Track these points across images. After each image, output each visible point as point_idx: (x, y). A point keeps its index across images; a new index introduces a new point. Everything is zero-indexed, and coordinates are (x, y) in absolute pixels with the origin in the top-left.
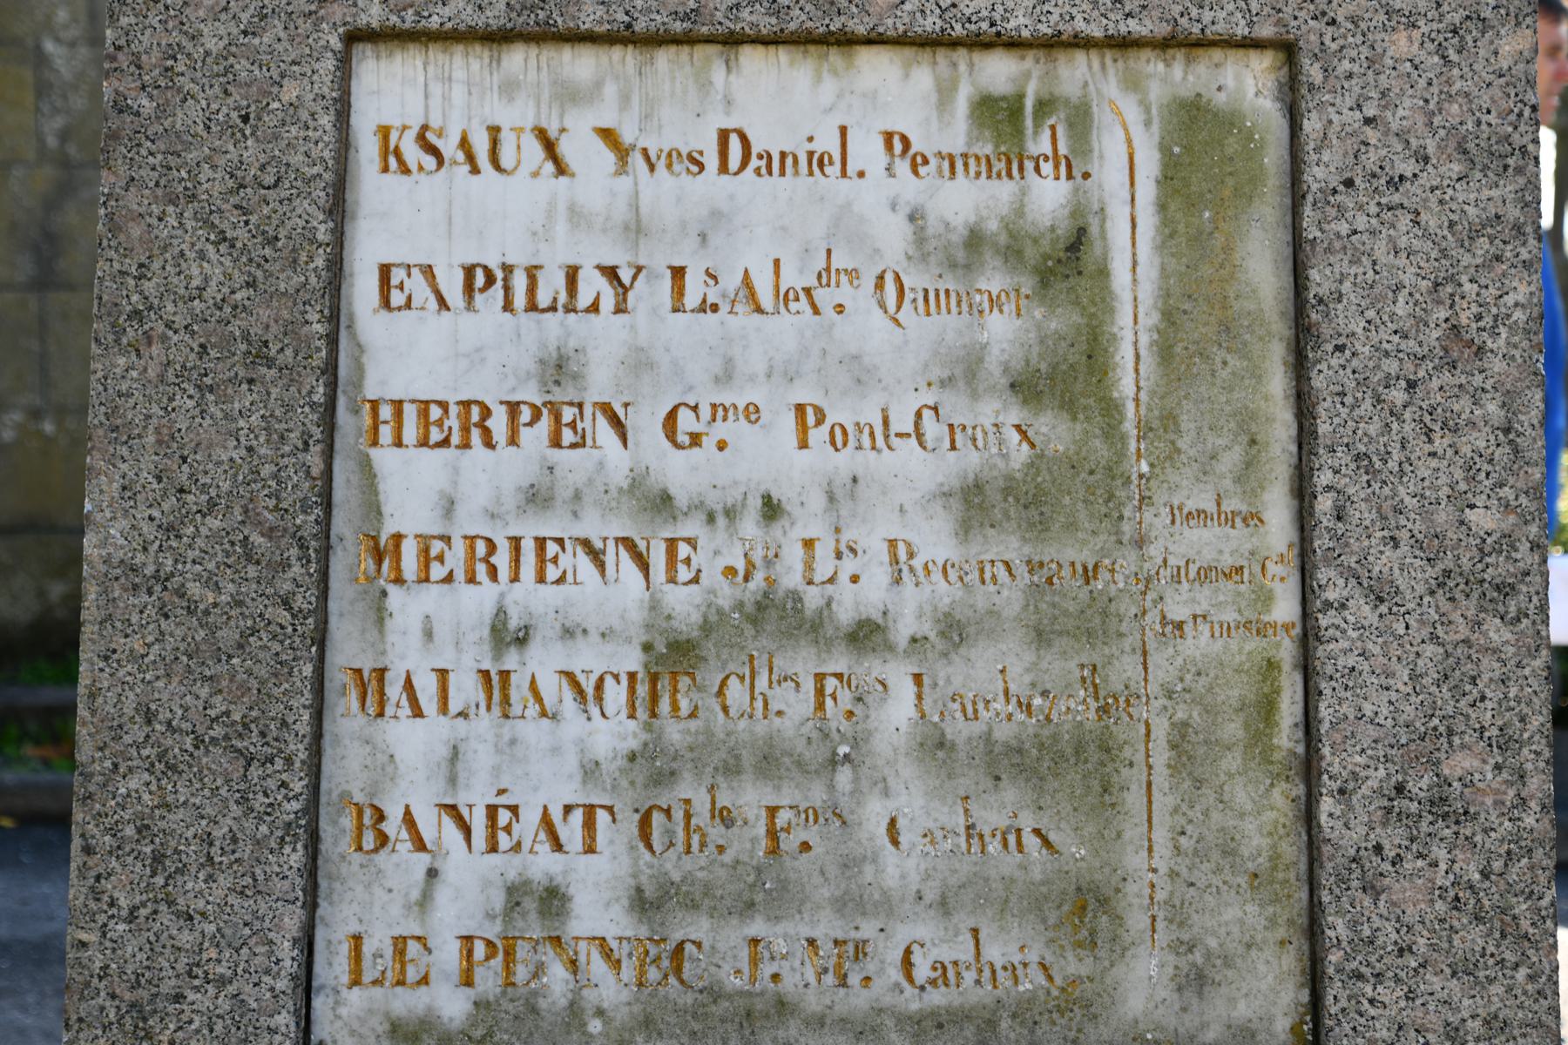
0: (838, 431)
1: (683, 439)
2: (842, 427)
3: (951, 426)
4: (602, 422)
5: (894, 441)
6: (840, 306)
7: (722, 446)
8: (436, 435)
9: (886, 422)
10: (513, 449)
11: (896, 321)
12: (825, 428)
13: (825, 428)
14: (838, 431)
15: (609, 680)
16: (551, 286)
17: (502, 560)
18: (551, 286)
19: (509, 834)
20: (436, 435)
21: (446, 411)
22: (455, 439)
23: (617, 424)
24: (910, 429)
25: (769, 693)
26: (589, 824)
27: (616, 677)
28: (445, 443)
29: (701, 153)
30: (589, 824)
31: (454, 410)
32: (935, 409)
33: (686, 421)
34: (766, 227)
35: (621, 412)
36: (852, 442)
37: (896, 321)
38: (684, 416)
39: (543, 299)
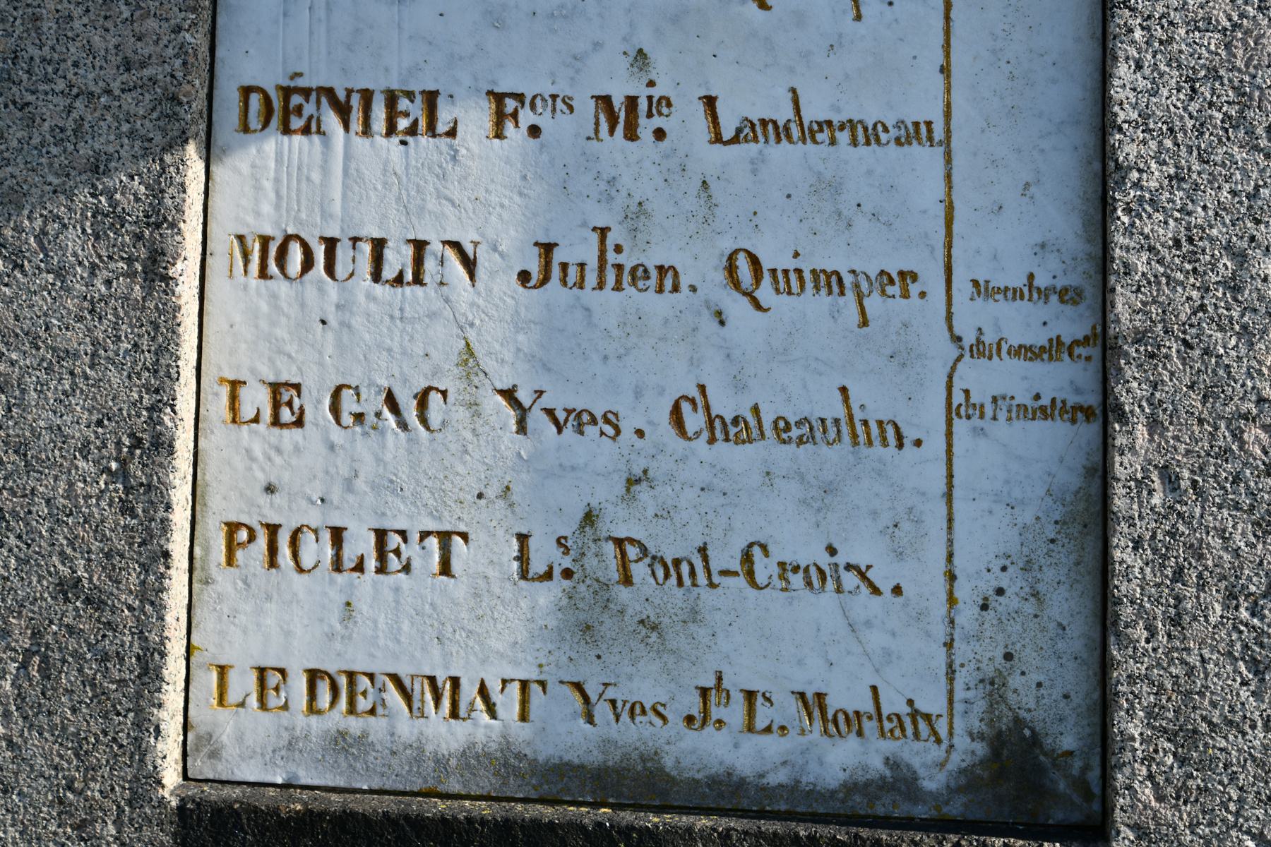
3: (782, 565)
24: (736, 565)
32: (764, 548)
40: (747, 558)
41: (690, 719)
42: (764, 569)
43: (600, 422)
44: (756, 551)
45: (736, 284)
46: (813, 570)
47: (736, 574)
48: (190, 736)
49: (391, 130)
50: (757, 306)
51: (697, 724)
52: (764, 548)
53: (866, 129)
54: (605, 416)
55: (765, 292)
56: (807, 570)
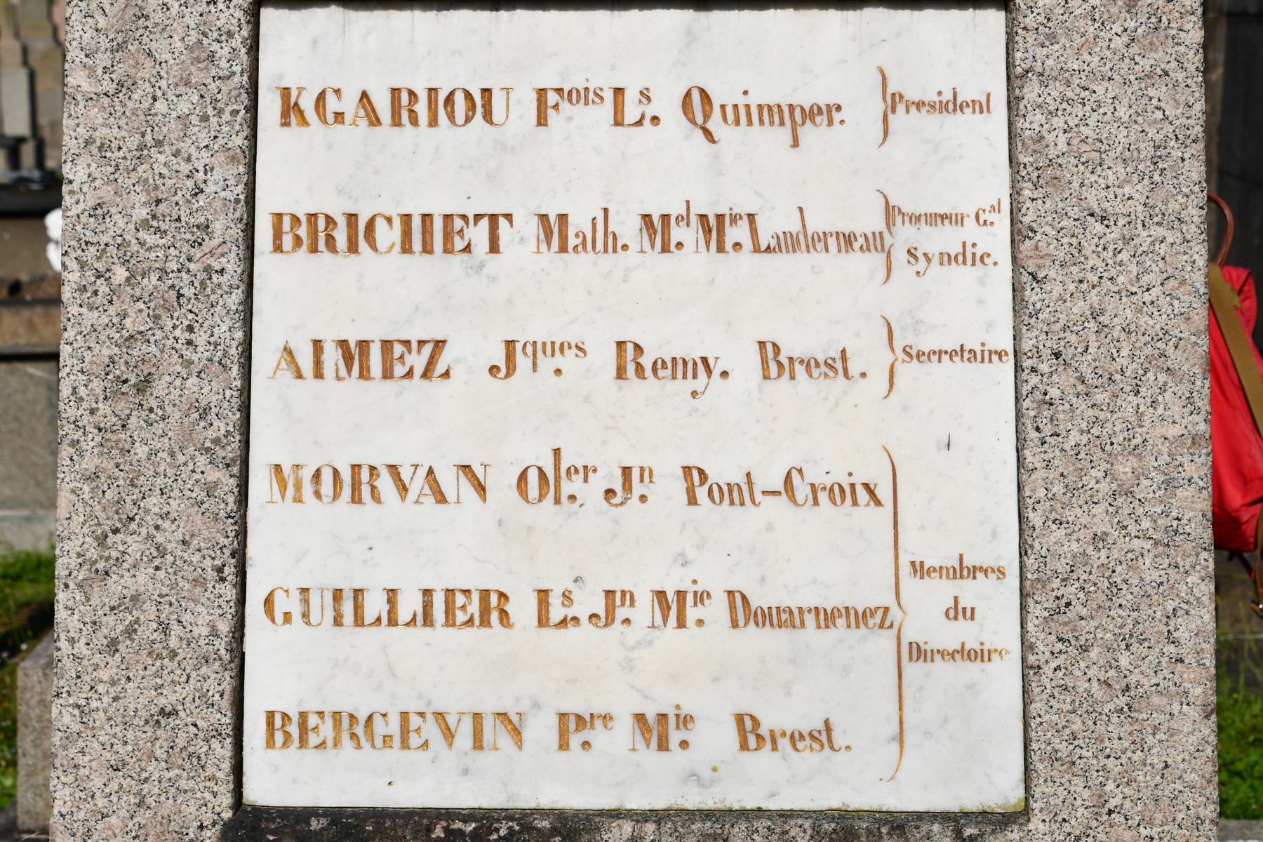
0: (715, 488)
2: (840, 486)
3: (813, 485)
5: (758, 497)
9: (750, 484)
10: (319, 381)
12: (706, 487)
13: (706, 487)
14: (715, 488)
16: (375, 605)
17: (422, 108)
18: (375, 605)
19: (462, 237)
22: (330, 743)
24: (780, 487)
31: (476, 597)
32: (800, 471)
34: (826, 181)
36: (307, 474)
39: (369, 617)
40: (788, 479)
41: (494, 370)
42: (802, 491)
43: (807, 738)
44: (795, 474)
45: (693, 121)
46: (836, 488)
47: (779, 493)
48: (1030, 562)
49: (387, 374)
50: (708, 134)
51: (617, 500)
52: (800, 471)
53: (856, 613)
54: (810, 734)
55: (715, 124)
56: (832, 489)
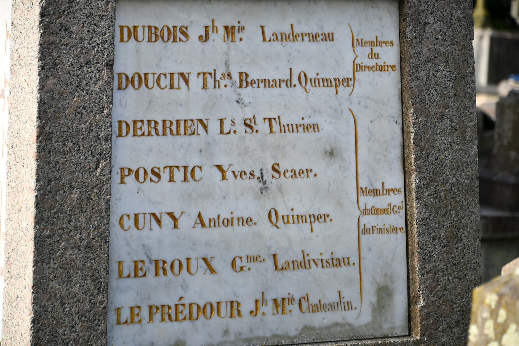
1: (238, 269)
4: (200, 126)
6: (263, 313)
7: (235, 132)
8: (139, 132)
11: (276, 226)
15: (162, 77)
20: (139, 132)
21: (143, 124)
22: (146, 133)
23: (205, 127)
25: (220, 80)
26: (171, 173)
27: (165, 75)
28: (143, 134)
29: (253, 171)
30: (171, 173)
31: (146, 123)
33: (238, 263)
35: (205, 122)
37: (276, 226)
38: (238, 260)
